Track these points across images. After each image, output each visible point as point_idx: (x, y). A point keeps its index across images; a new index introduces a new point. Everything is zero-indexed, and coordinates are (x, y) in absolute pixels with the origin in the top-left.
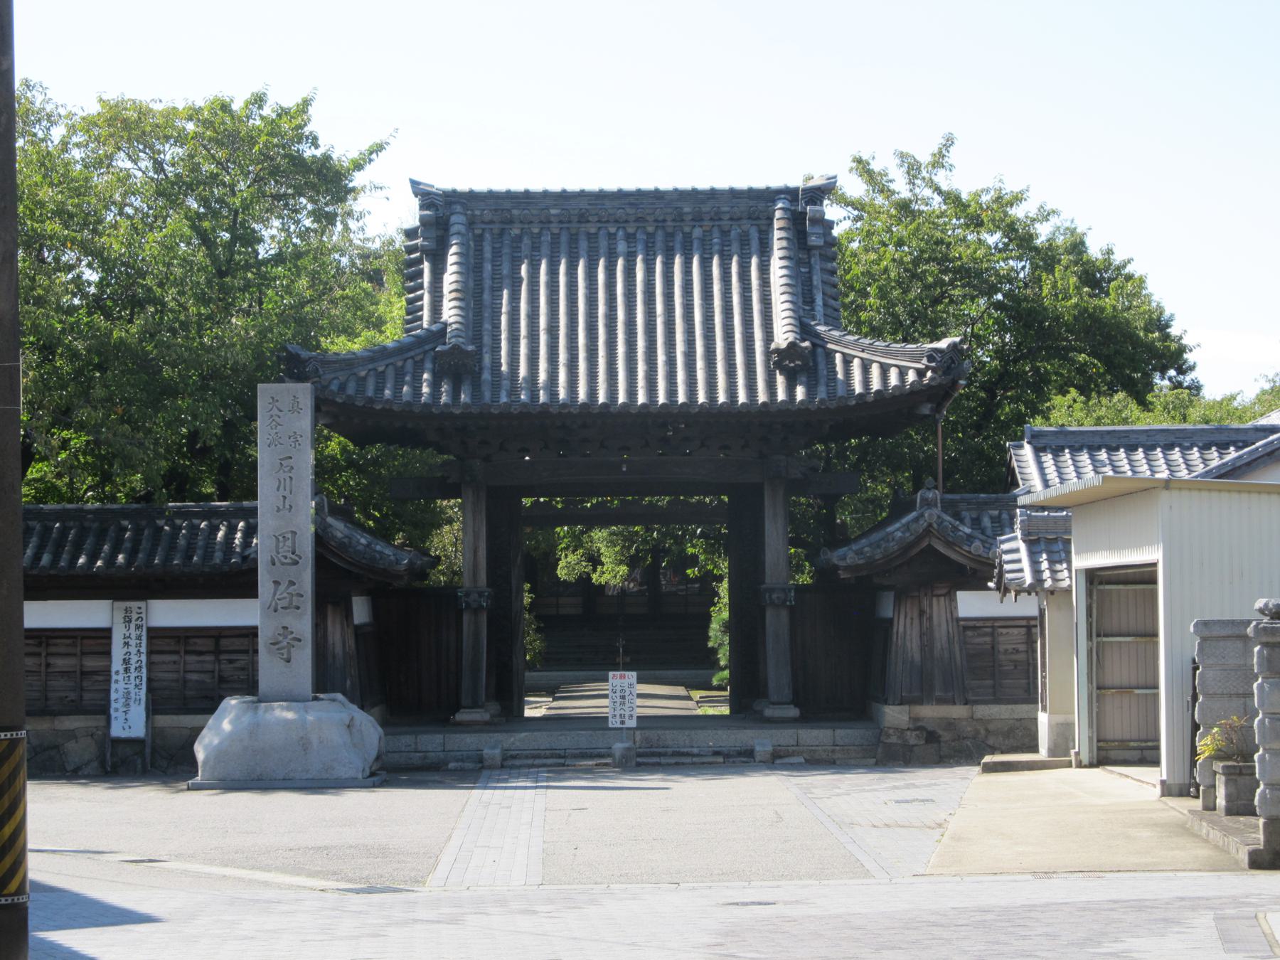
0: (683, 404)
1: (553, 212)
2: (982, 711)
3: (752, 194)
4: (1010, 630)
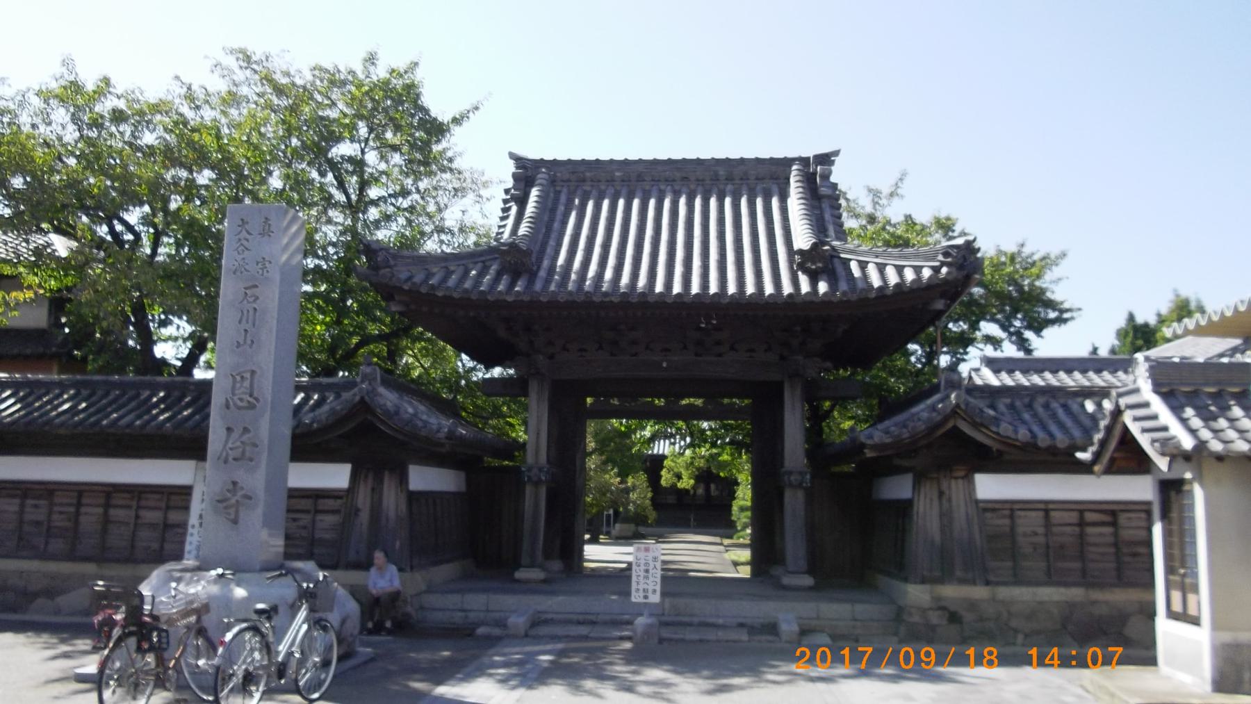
0: (715, 294)
1: (617, 174)
2: (1004, 592)
3: (773, 161)
4: (1029, 513)
